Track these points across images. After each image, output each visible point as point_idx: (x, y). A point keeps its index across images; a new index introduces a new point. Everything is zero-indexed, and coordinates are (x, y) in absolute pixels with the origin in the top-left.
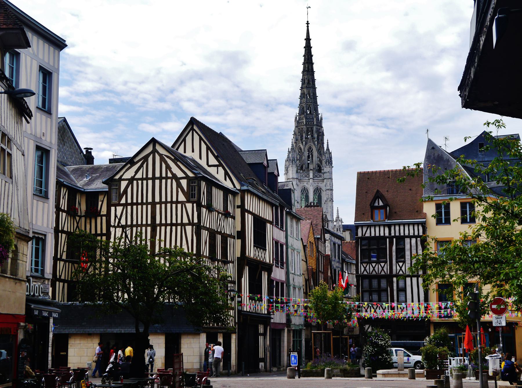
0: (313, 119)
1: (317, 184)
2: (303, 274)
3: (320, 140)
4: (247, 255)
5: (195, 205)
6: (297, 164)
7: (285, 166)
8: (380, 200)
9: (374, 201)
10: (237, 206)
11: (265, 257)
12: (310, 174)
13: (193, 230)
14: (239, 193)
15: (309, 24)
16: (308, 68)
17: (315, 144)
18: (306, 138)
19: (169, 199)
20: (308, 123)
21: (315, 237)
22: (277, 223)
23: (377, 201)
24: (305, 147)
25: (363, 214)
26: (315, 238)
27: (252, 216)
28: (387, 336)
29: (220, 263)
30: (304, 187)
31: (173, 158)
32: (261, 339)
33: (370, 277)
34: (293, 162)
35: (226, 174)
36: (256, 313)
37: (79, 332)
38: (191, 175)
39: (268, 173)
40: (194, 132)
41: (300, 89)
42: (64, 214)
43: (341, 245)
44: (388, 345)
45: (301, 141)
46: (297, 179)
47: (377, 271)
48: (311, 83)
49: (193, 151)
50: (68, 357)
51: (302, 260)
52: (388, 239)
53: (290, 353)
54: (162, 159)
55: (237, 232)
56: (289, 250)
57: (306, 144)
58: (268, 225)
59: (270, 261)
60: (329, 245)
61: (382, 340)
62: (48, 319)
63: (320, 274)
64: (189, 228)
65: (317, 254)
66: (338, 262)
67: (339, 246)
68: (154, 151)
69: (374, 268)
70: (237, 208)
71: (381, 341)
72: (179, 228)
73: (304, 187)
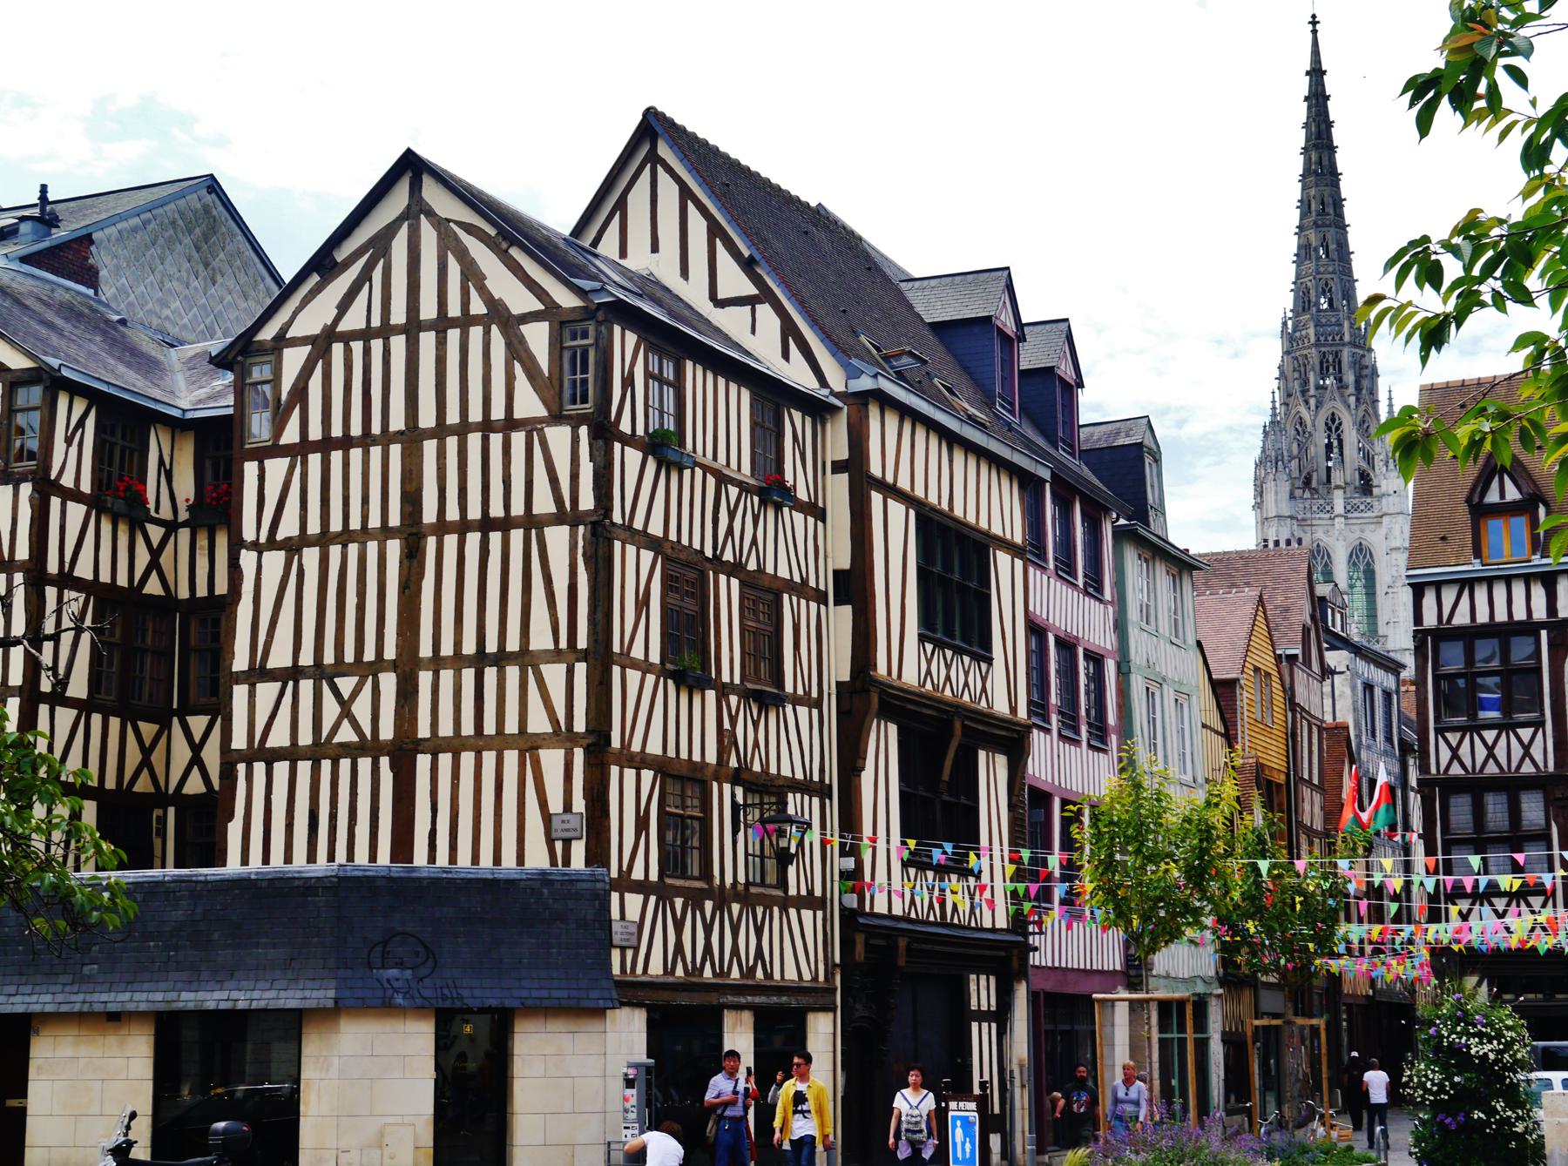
0: (1341, 325)
1: (1358, 534)
2: (1207, 781)
3: (1364, 391)
4: (882, 669)
5: (583, 431)
6: (1290, 471)
7: (1256, 479)
9: (1483, 482)
10: (833, 462)
11: (984, 690)
12: (1335, 502)
13: (577, 543)
15: (1318, 22)
17: (1349, 406)
18: (1318, 387)
19: (475, 415)
21: (1278, 652)
22: (1068, 565)
23: (1495, 484)
24: (1316, 416)
25: (1443, 539)
26: (1278, 658)
27: (912, 513)
28: (1510, 1016)
29: (734, 699)
31: (492, 232)
32: (981, 1036)
33: (1476, 786)
34: (1277, 463)
35: (789, 330)
36: (943, 924)
37: (64, 1008)
38: (566, 299)
39: (1022, 373)
40: (659, 168)
41: (1296, 234)
42: (76, 511)
43: (1398, 692)
44: (1516, 1061)
45: (1303, 396)
46: (1292, 517)
47: (1503, 761)
48: (1331, 212)
49: (655, 248)
50: (28, 1119)
51: (1204, 726)
52: (1544, 633)
53: (947, 1105)
54: (449, 242)
55: (837, 573)
56: (1137, 685)
58: (1003, 559)
59: (1013, 710)
60: (1348, 691)
62: (1533, 1047)
63: (1306, 792)
64: (557, 538)
65: (1290, 715)
66: (1385, 753)
67: (1387, 695)
68: (417, 209)
69: (1490, 750)
70: (833, 472)
72: (517, 536)
73: (1318, 545)
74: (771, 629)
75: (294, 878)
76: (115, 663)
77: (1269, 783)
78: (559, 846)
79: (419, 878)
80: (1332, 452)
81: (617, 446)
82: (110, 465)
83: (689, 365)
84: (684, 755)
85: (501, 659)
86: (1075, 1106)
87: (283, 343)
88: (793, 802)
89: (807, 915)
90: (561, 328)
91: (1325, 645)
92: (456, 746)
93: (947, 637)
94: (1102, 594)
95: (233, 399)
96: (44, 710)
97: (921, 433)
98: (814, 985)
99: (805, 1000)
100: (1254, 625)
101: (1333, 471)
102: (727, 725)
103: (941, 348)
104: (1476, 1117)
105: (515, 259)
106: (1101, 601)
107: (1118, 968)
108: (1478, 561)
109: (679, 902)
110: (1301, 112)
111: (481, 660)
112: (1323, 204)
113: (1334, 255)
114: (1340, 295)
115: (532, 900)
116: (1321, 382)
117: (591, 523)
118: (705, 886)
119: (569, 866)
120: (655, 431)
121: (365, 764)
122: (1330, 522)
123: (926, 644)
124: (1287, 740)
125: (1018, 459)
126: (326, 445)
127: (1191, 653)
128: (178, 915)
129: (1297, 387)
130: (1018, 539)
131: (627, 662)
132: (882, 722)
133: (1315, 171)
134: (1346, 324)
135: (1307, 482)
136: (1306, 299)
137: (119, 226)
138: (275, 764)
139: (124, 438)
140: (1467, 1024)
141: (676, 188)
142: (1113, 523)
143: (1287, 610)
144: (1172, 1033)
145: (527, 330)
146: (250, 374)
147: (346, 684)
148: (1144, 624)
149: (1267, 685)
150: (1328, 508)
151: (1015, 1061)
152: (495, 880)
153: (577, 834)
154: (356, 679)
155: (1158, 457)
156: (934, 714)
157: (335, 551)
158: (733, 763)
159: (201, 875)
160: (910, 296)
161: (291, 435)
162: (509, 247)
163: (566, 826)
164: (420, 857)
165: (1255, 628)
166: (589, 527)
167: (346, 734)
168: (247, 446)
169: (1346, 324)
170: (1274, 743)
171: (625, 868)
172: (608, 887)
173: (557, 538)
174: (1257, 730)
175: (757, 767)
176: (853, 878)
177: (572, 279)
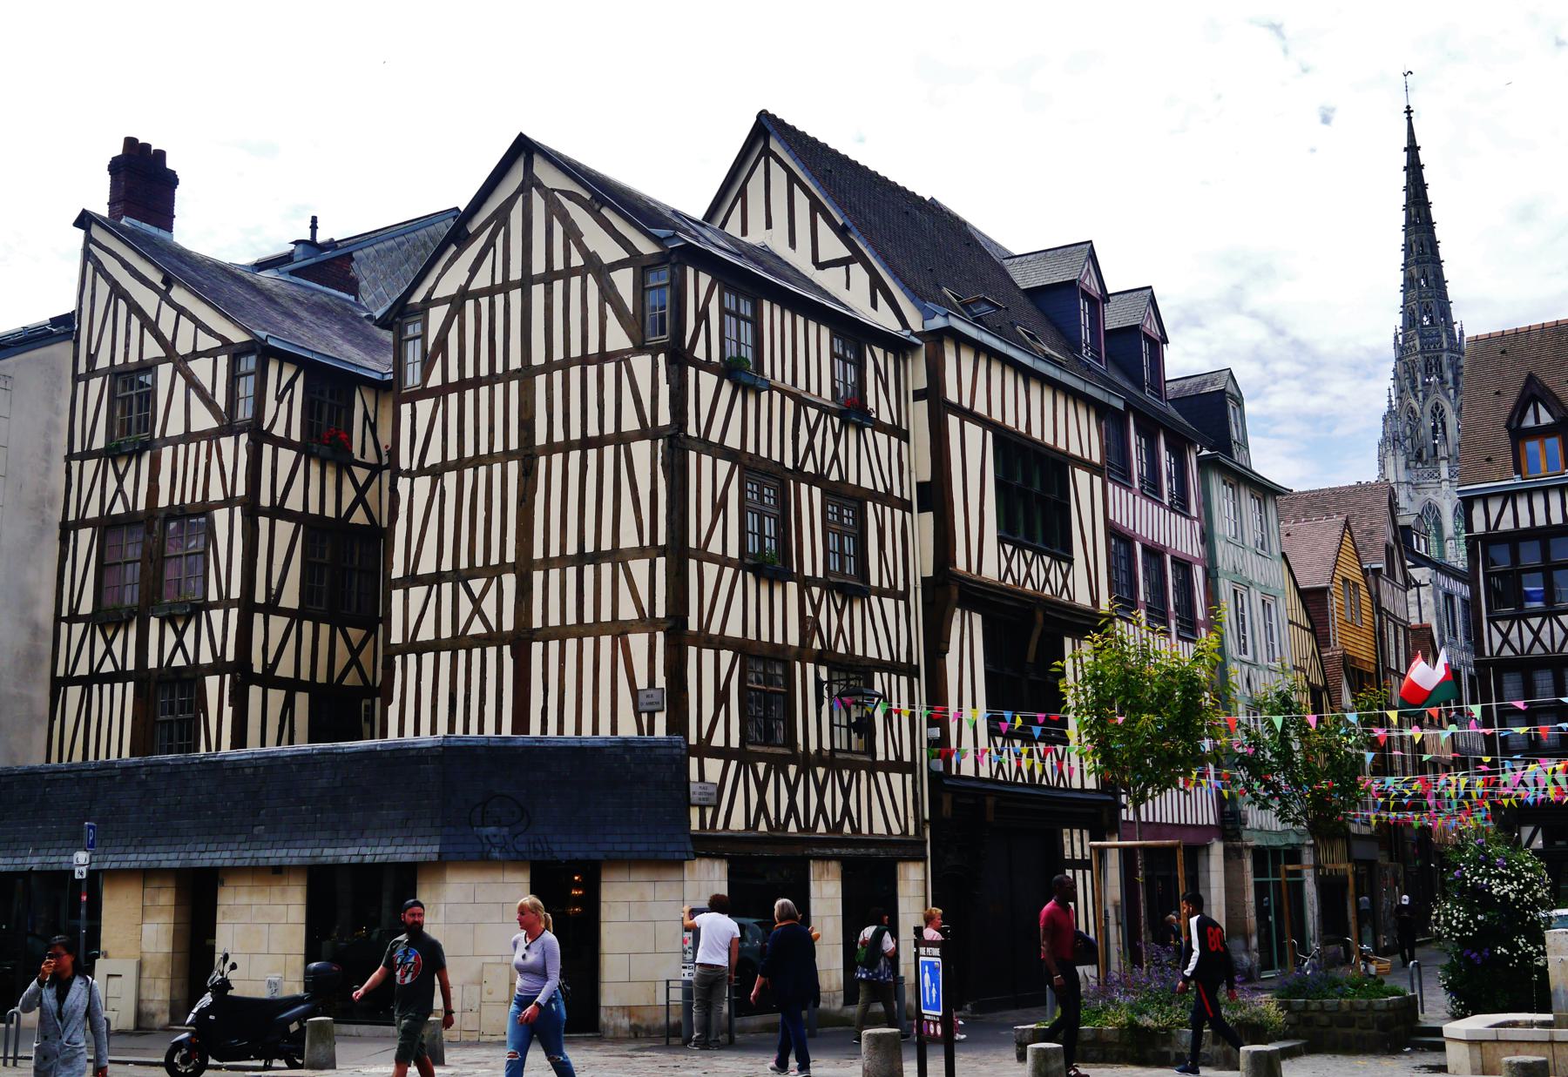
0: (1440, 336)
4: (961, 564)
5: (661, 358)
7: (1379, 456)
8: (1540, 406)
10: (914, 392)
11: (1065, 585)
13: (657, 454)
14: (920, 346)
15: (1412, 111)
16: (1418, 215)
17: (1449, 397)
18: (1424, 384)
20: (1426, 347)
21: (1364, 567)
22: (1154, 487)
23: (1530, 412)
24: (1423, 406)
25: (1489, 460)
27: (989, 434)
29: (816, 591)
30: (1430, 503)
31: (587, 196)
35: (877, 284)
37: (239, 863)
38: (646, 247)
40: (771, 160)
41: (1402, 270)
44: (1537, 901)
45: (1413, 391)
46: (1408, 483)
47: (1547, 643)
48: (1429, 251)
49: (769, 226)
51: (1291, 622)
54: (554, 209)
55: (919, 485)
56: (1225, 588)
57: (1425, 397)
58: (1082, 476)
59: (1095, 602)
60: (1431, 600)
61: (1507, 876)
64: (641, 450)
65: (1377, 617)
68: (530, 182)
71: (1502, 880)
72: (609, 451)
73: (1430, 503)
74: (856, 532)
75: (409, 749)
76: (325, 579)
77: (1360, 672)
78: (645, 717)
79: (515, 747)
80: (1437, 433)
81: (691, 371)
82: (320, 418)
83: (766, 305)
84: (765, 637)
85: (597, 557)
86: (398, 973)
87: (430, 303)
88: (879, 682)
89: (896, 778)
90: (643, 272)
91: (1409, 563)
92: (562, 634)
93: (1064, 551)
94: (1189, 511)
95: (391, 357)
96: (258, 619)
97: (996, 370)
98: (903, 838)
99: (894, 852)
100: (1341, 544)
101: (1438, 446)
102: (809, 612)
103: (1030, 306)
104: (1499, 952)
105: (606, 218)
106: (1187, 517)
107: (1212, 822)
108: (1519, 476)
109: (761, 767)
110: (1402, 179)
111: (581, 559)
112: (1422, 246)
113: (1432, 284)
114: (1438, 313)
115: (616, 765)
116: (1427, 380)
117: (668, 436)
118: (788, 752)
119: (653, 735)
120: (729, 358)
121: (491, 652)
122: (1438, 485)
123: (1006, 546)
124: (1375, 637)
125: (1090, 390)
126: (462, 385)
127: (1277, 563)
128: (322, 783)
129: (1407, 384)
130: (1096, 459)
131: (703, 555)
132: (967, 612)
133: (1415, 222)
134: (1444, 335)
135: (1419, 457)
136: (1412, 318)
137: (376, 247)
138: (424, 655)
139: (331, 397)
140: (1489, 866)
141: (785, 174)
142: (1197, 453)
143: (1372, 533)
144: (1268, 877)
145: (616, 276)
146: (406, 331)
147: (477, 585)
148: (1259, 550)
149: (1355, 593)
150: (1436, 475)
151: (1109, 902)
152: (582, 747)
153: (659, 707)
154: (484, 580)
155: (1240, 402)
156: (1016, 605)
157: (469, 473)
158: (817, 645)
159: (340, 748)
160: (1010, 270)
161: (435, 380)
162: (600, 208)
163: (650, 700)
164: (535, 730)
165: (1343, 546)
166: (666, 440)
167: (477, 628)
168: (404, 391)
169: (1444, 335)
170: (1363, 639)
171: (704, 736)
172: (684, 753)
173: (641, 450)
174: (1347, 629)
175: (841, 649)
176: (940, 746)
177: (650, 230)
